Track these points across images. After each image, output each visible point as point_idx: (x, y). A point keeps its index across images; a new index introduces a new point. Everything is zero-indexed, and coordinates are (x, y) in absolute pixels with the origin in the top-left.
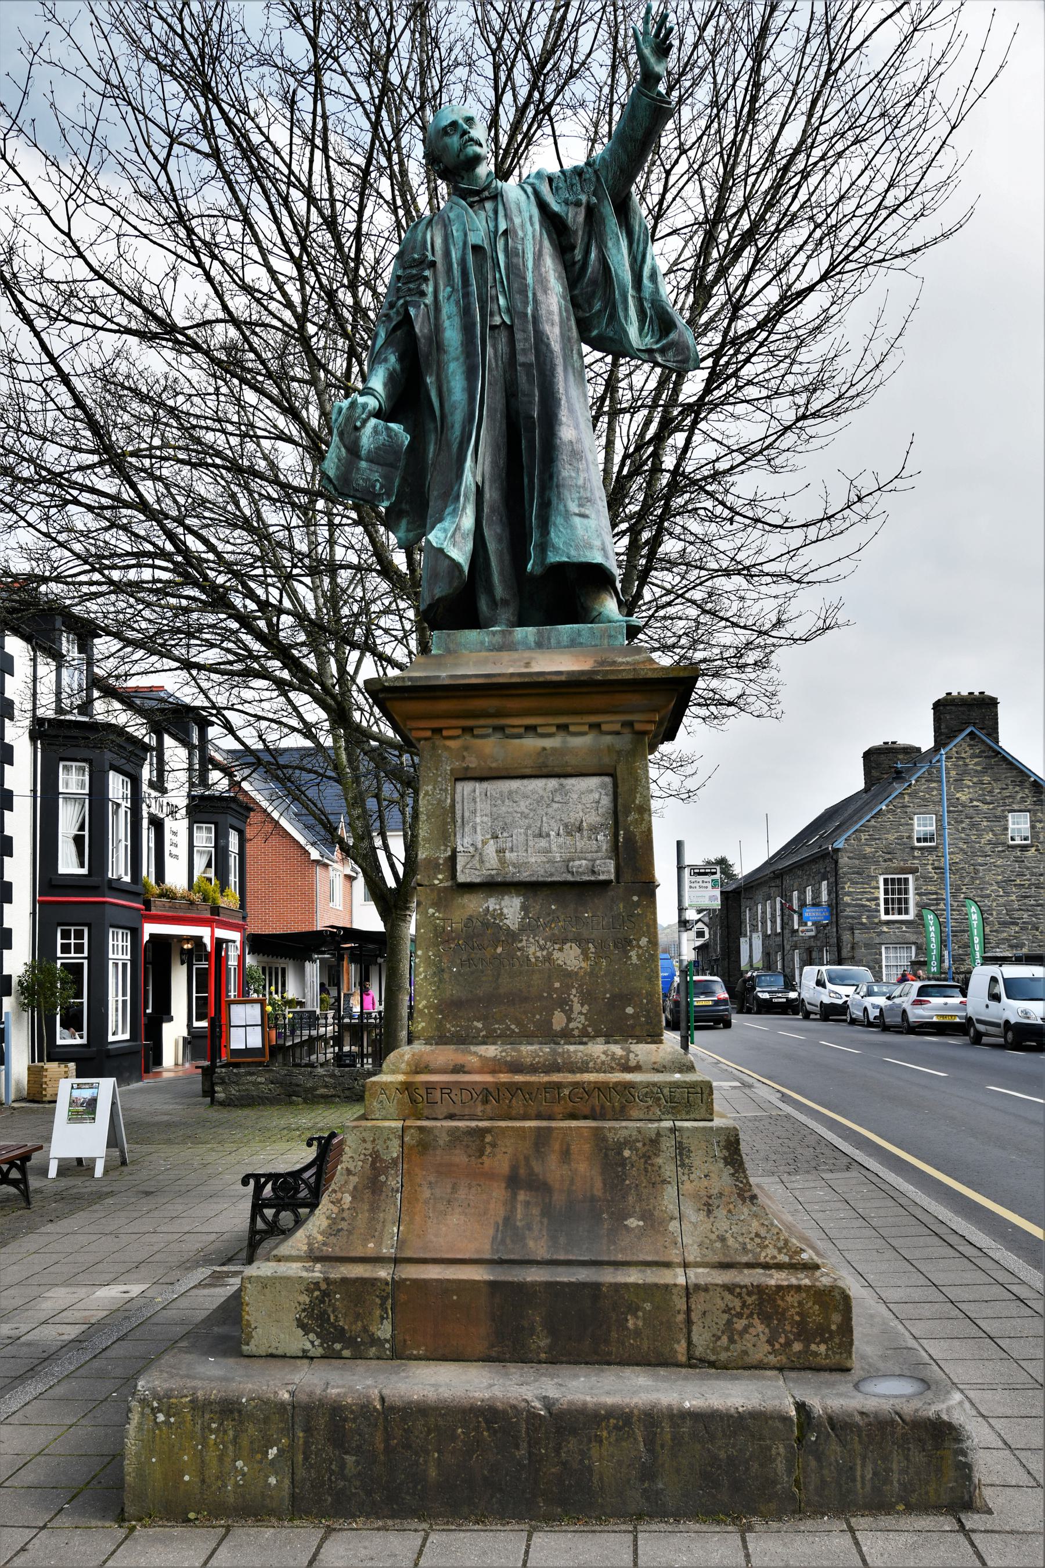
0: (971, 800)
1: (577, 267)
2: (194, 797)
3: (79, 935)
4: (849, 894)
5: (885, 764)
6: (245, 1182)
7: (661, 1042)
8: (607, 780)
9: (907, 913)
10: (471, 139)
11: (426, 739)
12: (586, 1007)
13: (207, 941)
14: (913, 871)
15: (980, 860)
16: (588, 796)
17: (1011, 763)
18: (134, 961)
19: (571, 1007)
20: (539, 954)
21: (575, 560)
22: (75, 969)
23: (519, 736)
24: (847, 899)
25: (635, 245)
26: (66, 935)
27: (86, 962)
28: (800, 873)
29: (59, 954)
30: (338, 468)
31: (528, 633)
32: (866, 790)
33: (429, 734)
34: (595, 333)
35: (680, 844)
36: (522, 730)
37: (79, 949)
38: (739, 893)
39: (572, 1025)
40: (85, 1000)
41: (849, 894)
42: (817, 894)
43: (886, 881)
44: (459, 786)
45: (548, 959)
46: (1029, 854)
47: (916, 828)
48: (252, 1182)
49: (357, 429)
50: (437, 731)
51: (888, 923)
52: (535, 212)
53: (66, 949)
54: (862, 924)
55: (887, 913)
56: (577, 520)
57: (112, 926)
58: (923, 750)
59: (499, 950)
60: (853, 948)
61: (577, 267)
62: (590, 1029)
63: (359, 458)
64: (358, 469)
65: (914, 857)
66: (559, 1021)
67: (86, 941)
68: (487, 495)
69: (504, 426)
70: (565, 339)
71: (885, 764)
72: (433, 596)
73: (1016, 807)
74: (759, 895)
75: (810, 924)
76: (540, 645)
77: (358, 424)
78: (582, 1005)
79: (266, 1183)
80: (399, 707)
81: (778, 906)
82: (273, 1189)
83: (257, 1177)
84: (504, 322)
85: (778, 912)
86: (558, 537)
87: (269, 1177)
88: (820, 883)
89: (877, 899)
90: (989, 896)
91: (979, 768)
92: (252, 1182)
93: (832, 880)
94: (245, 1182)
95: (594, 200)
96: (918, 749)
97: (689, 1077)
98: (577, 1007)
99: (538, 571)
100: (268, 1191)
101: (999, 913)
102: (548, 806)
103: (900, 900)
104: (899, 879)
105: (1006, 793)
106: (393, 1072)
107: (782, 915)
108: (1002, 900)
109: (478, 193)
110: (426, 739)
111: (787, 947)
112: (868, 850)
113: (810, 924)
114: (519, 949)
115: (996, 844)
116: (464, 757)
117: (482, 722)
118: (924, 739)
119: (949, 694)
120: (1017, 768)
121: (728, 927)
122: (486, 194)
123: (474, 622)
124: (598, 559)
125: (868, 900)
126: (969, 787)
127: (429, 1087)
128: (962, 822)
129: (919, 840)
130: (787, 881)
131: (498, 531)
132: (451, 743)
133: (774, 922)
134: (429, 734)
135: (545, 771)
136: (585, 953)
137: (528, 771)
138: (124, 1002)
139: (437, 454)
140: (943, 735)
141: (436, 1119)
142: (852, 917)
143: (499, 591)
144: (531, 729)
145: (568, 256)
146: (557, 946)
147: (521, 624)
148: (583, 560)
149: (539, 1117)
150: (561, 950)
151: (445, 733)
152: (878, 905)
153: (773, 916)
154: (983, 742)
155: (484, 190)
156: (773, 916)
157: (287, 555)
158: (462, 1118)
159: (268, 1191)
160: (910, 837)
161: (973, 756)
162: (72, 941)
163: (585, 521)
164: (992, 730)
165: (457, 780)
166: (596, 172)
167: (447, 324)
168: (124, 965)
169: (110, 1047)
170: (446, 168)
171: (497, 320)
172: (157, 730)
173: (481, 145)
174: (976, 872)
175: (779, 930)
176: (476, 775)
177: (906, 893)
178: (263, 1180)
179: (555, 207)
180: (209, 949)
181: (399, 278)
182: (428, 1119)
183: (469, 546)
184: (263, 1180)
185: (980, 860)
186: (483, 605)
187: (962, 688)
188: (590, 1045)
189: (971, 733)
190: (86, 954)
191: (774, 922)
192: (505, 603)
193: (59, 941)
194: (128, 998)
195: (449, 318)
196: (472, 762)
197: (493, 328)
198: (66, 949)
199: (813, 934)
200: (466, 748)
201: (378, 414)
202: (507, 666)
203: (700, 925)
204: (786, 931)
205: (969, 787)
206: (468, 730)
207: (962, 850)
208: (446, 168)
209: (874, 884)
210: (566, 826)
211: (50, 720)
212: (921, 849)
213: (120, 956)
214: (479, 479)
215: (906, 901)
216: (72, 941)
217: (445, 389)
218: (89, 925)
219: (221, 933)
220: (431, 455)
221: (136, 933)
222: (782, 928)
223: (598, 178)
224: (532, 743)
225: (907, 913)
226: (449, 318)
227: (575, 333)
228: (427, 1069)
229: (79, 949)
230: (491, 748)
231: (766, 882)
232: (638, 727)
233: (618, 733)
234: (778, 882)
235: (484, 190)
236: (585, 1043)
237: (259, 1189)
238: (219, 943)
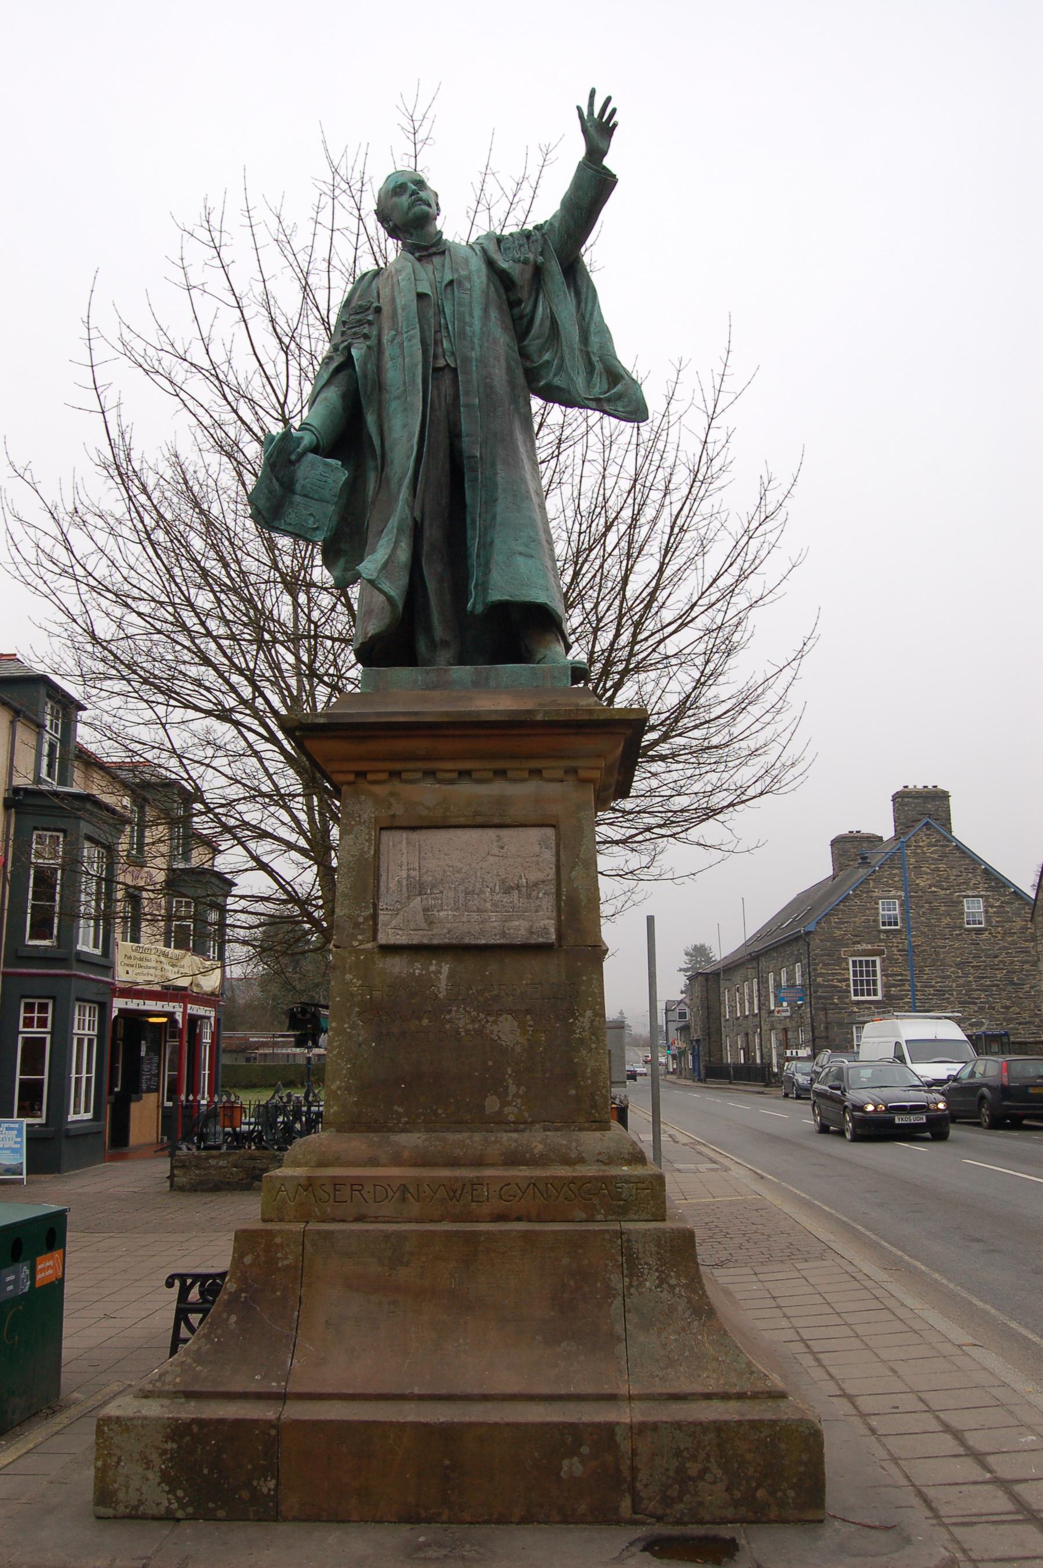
0: (930, 886)
1: (525, 320)
2: (174, 870)
3: (43, 1008)
4: (821, 975)
5: (850, 849)
6: (170, 1284)
7: (609, 1130)
8: (550, 832)
9: (875, 994)
10: (420, 199)
11: (349, 783)
12: (523, 1088)
13: (179, 1017)
14: (879, 953)
15: (940, 943)
16: (529, 851)
17: (964, 852)
18: (100, 1036)
19: (506, 1088)
20: (470, 1027)
21: (517, 599)
22: (34, 1047)
23: (452, 782)
24: (819, 979)
25: (583, 305)
26: (29, 1008)
27: (48, 1037)
28: (775, 955)
29: (21, 1029)
30: (268, 499)
31: (463, 672)
32: (834, 877)
33: (351, 777)
34: (542, 383)
35: (650, 920)
36: (455, 775)
37: (42, 1023)
38: (718, 974)
39: (507, 1110)
40: (46, 1077)
41: (821, 975)
42: (791, 976)
43: (854, 962)
44: (386, 836)
45: (480, 1032)
46: (984, 937)
47: (881, 912)
48: (177, 1283)
49: (292, 463)
50: (361, 774)
51: (858, 1003)
52: (483, 268)
53: (29, 1022)
54: (834, 1004)
55: (856, 995)
56: (520, 560)
57: (78, 999)
58: (885, 839)
59: (425, 1022)
60: (826, 1028)
61: (525, 320)
62: (526, 1115)
63: (293, 492)
64: (291, 503)
65: (881, 941)
66: (492, 1104)
67: (50, 1015)
68: (427, 533)
69: (447, 466)
70: (512, 383)
71: (850, 849)
72: (366, 633)
73: (970, 893)
74: (737, 977)
75: (785, 1004)
76: (476, 684)
77: (293, 457)
78: (518, 1086)
79: (192, 1285)
80: (321, 747)
81: (755, 987)
82: (201, 1293)
83: (182, 1277)
84: (448, 365)
85: (755, 994)
86: (496, 577)
87: (196, 1277)
88: (794, 965)
89: (848, 979)
90: (949, 977)
91: (935, 856)
92: (177, 1283)
93: (805, 961)
94: (170, 1284)
95: (540, 259)
96: (880, 839)
97: (639, 1171)
98: (512, 1089)
99: (480, 609)
100: (194, 1295)
101: (959, 993)
102: (483, 859)
103: (868, 981)
104: (867, 962)
105: (961, 880)
106: (298, 1165)
107: (759, 996)
108: (961, 981)
109: (426, 248)
110: (349, 783)
111: (764, 1027)
112: (838, 933)
113: (785, 1004)
114: (448, 1021)
115: (955, 928)
116: (390, 804)
117: (411, 765)
118: (885, 827)
119: (906, 787)
120: (969, 857)
121: (708, 1008)
122: (434, 250)
123: (410, 660)
124: (541, 598)
125: (840, 981)
126: (927, 874)
127: (337, 1183)
128: (923, 907)
129: (884, 924)
130: (763, 963)
131: (439, 570)
132: (376, 789)
133: (751, 1003)
134: (351, 777)
135: (479, 820)
136: (522, 1025)
137: (462, 821)
138: (88, 1080)
139: (377, 493)
140: (903, 823)
141: (344, 1221)
142: (825, 998)
143: (439, 632)
144: (464, 774)
145: (516, 311)
146: (490, 1019)
147: (461, 663)
148: (528, 599)
149: (456, 1219)
150: (495, 1022)
151: (370, 777)
152: (848, 986)
153: (751, 997)
154: (938, 832)
155: (432, 246)
156: (751, 997)
157: (281, 639)
158: (376, 1220)
159: (194, 1295)
160: (876, 921)
161: (930, 845)
162: (36, 1015)
163: (530, 561)
164: (946, 821)
165: (382, 829)
166: (543, 235)
167: (389, 364)
168: (90, 1041)
169: (70, 1127)
170: (395, 225)
171: (441, 363)
172: (140, 802)
173: (429, 205)
174: (937, 953)
175: (756, 1011)
176: (405, 824)
177: (875, 975)
178: (189, 1281)
179: (504, 265)
180: (181, 1026)
181: (344, 323)
182: (334, 1220)
183: (404, 580)
184: (189, 1281)
185: (940, 943)
186: (422, 647)
187: (918, 781)
188: (526, 1134)
189: (927, 824)
190: (49, 1029)
191: (751, 1003)
192: (445, 644)
193: (22, 1015)
194: (93, 1075)
195: (392, 359)
196: (398, 809)
197: (436, 370)
198: (29, 1022)
199: (788, 1014)
200: (392, 794)
201: (315, 449)
202: (436, 705)
203: (682, 1006)
204: (763, 1012)
205: (927, 874)
206: (395, 774)
207: (923, 933)
208: (395, 225)
209: (844, 965)
210: (503, 881)
211: (26, 790)
212: (886, 932)
213: (86, 1032)
214: (417, 514)
215: (875, 982)
216: (36, 1015)
217: (386, 427)
218: (54, 998)
219: (195, 1009)
220: (371, 493)
221: (104, 1008)
222: (759, 1009)
223: (545, 241)
224: (466, 789)
225: (875, 994)
226: (392, 359)
227: (521, 380)
228: (335, 1161)
229: (42, 1023)
230: (426, 794)
231: (743, 964)
232: (583, 774)
233: (562, 781)
234: (755, 964)
235: (432, 246)
236: (523, 1131)
237: (184, 1291)
238: (193, 1021)
